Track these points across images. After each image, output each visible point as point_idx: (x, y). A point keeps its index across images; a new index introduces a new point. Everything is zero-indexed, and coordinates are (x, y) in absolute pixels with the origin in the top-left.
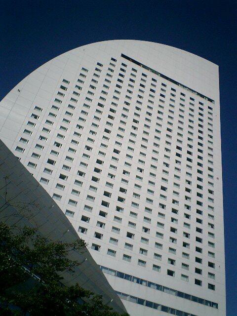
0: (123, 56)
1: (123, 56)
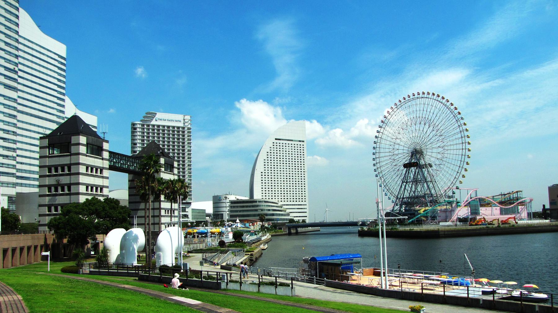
0: (276, 139)
1: (276, 139)
